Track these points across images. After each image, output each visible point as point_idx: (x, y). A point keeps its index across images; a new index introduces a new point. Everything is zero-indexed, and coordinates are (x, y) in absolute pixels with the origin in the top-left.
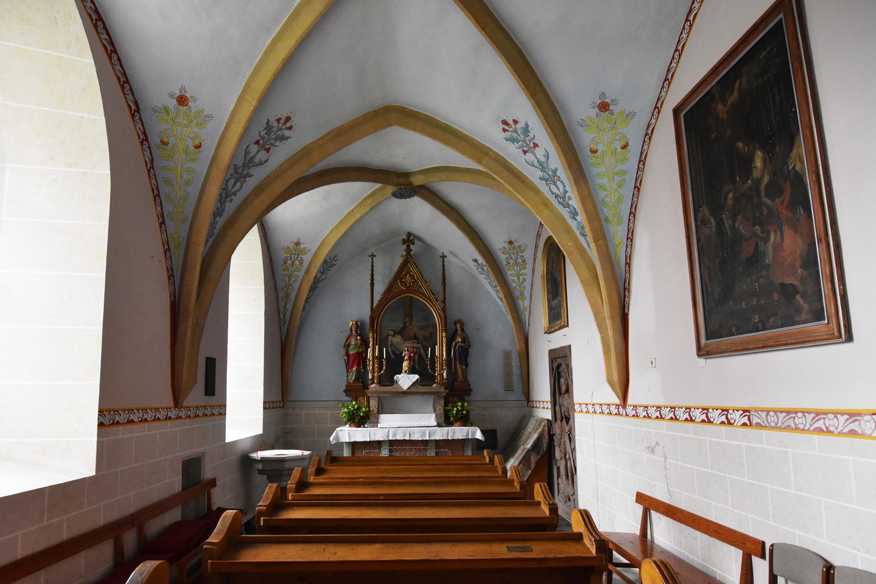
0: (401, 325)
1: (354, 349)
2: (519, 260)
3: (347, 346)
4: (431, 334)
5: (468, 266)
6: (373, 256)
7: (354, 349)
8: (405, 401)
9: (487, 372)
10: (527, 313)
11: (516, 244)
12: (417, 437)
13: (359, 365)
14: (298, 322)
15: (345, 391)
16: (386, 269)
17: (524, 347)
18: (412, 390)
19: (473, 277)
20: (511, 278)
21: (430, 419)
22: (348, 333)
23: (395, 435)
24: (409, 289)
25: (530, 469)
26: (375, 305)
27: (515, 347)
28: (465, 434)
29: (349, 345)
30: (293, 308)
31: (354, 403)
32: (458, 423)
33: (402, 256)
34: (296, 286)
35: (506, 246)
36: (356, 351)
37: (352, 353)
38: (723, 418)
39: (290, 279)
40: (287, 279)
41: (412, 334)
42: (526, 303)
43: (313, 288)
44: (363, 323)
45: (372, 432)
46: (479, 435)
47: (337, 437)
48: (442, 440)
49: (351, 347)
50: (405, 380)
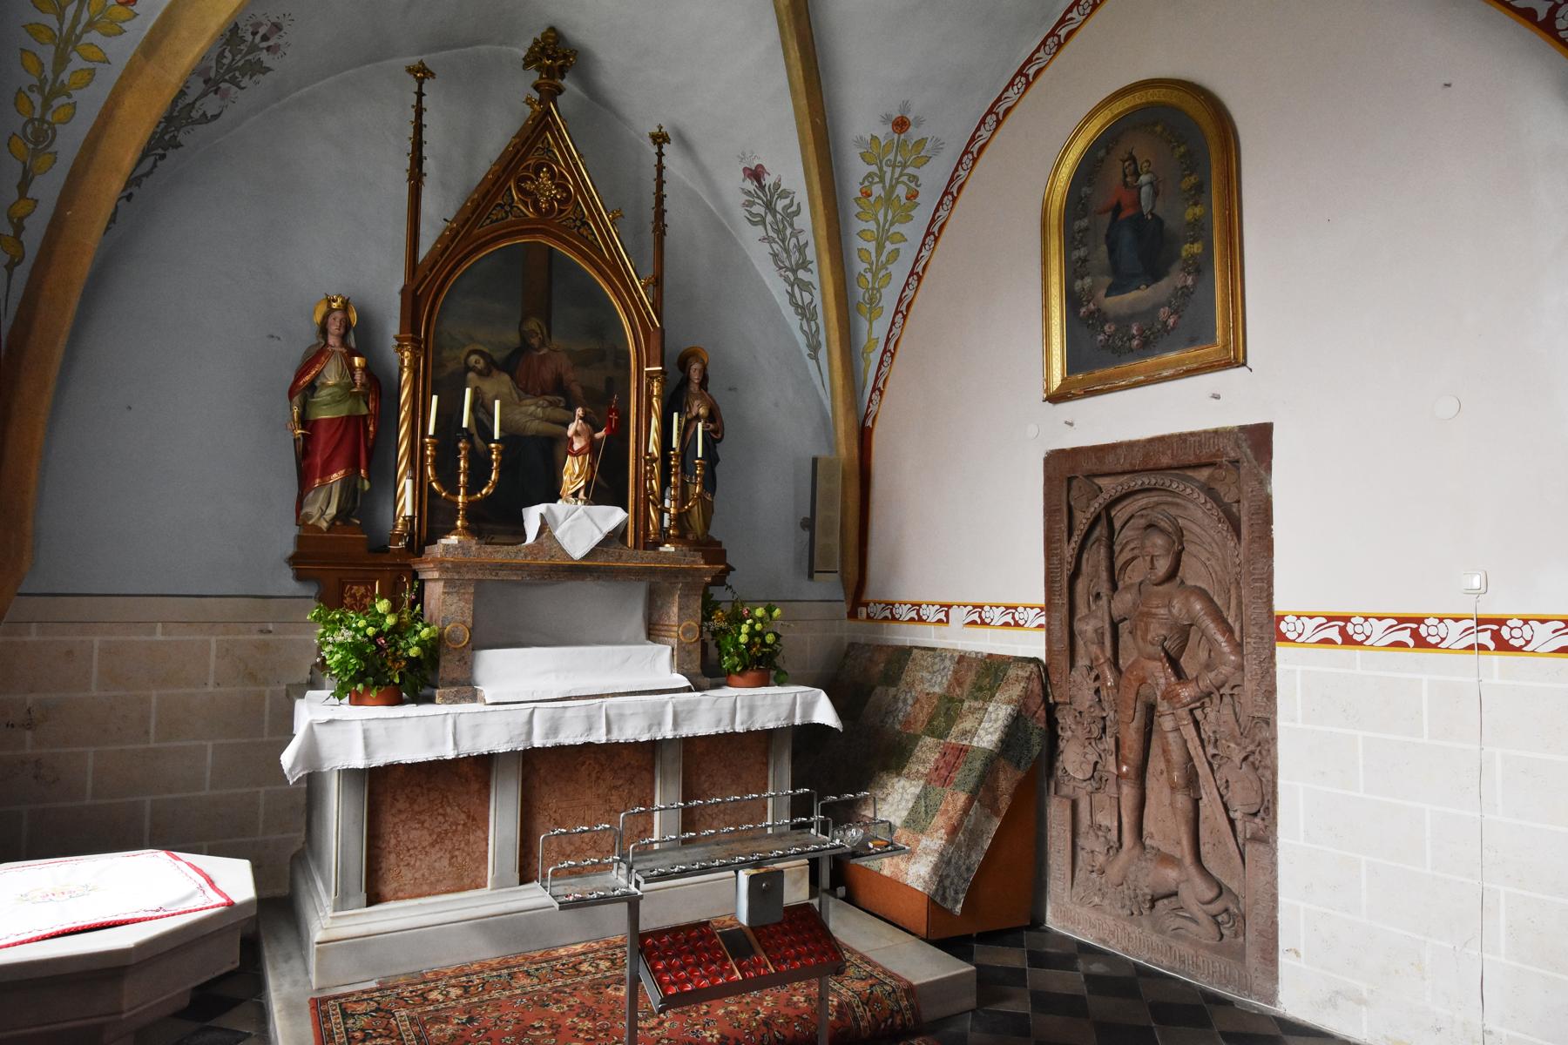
0: (513, 338)
1: (336, 401)
2: (901, 191)
3: (304, 390)
4: (610, 381)
5: (716, 194)
6: (422, 73)
7: (336, 401)
8: (549, 602)
9: (765, 508)
10: (875, 358)
11: (914, 133)
12: (633, 731)
13: (353, 465)
14: (83, 268)
15: (294, 561)
16: (475, 132)
17: (856, 451)
18: (600, 562)
19: (722, 232)
20: (859, 243)
21: (656, 665)
22: (310, 338)
23: (554, 729)
24: (547, 221)
25: (997, 814)
26: (423, 251)
27: (845, 449)
28: (784, 712)
29: (312, 387)
30: (57, 224)
31: (382, 606)
32: (751, 675)
33: (529, 102)
34: (90, 101)
35: (884, 132)
36: (342, 411)
37: (324, 414)
38: (913, 614)
39: (61, 61)
40: (47, 53)
41: (547, 374)
42: (880, 328)
43: (162, 143)
44: (356, 331)
45: (464, 724)
46: (824, 713)
47: (311, 752)
48: (717, 737)
49: (323, 395)
50: (577, 525)
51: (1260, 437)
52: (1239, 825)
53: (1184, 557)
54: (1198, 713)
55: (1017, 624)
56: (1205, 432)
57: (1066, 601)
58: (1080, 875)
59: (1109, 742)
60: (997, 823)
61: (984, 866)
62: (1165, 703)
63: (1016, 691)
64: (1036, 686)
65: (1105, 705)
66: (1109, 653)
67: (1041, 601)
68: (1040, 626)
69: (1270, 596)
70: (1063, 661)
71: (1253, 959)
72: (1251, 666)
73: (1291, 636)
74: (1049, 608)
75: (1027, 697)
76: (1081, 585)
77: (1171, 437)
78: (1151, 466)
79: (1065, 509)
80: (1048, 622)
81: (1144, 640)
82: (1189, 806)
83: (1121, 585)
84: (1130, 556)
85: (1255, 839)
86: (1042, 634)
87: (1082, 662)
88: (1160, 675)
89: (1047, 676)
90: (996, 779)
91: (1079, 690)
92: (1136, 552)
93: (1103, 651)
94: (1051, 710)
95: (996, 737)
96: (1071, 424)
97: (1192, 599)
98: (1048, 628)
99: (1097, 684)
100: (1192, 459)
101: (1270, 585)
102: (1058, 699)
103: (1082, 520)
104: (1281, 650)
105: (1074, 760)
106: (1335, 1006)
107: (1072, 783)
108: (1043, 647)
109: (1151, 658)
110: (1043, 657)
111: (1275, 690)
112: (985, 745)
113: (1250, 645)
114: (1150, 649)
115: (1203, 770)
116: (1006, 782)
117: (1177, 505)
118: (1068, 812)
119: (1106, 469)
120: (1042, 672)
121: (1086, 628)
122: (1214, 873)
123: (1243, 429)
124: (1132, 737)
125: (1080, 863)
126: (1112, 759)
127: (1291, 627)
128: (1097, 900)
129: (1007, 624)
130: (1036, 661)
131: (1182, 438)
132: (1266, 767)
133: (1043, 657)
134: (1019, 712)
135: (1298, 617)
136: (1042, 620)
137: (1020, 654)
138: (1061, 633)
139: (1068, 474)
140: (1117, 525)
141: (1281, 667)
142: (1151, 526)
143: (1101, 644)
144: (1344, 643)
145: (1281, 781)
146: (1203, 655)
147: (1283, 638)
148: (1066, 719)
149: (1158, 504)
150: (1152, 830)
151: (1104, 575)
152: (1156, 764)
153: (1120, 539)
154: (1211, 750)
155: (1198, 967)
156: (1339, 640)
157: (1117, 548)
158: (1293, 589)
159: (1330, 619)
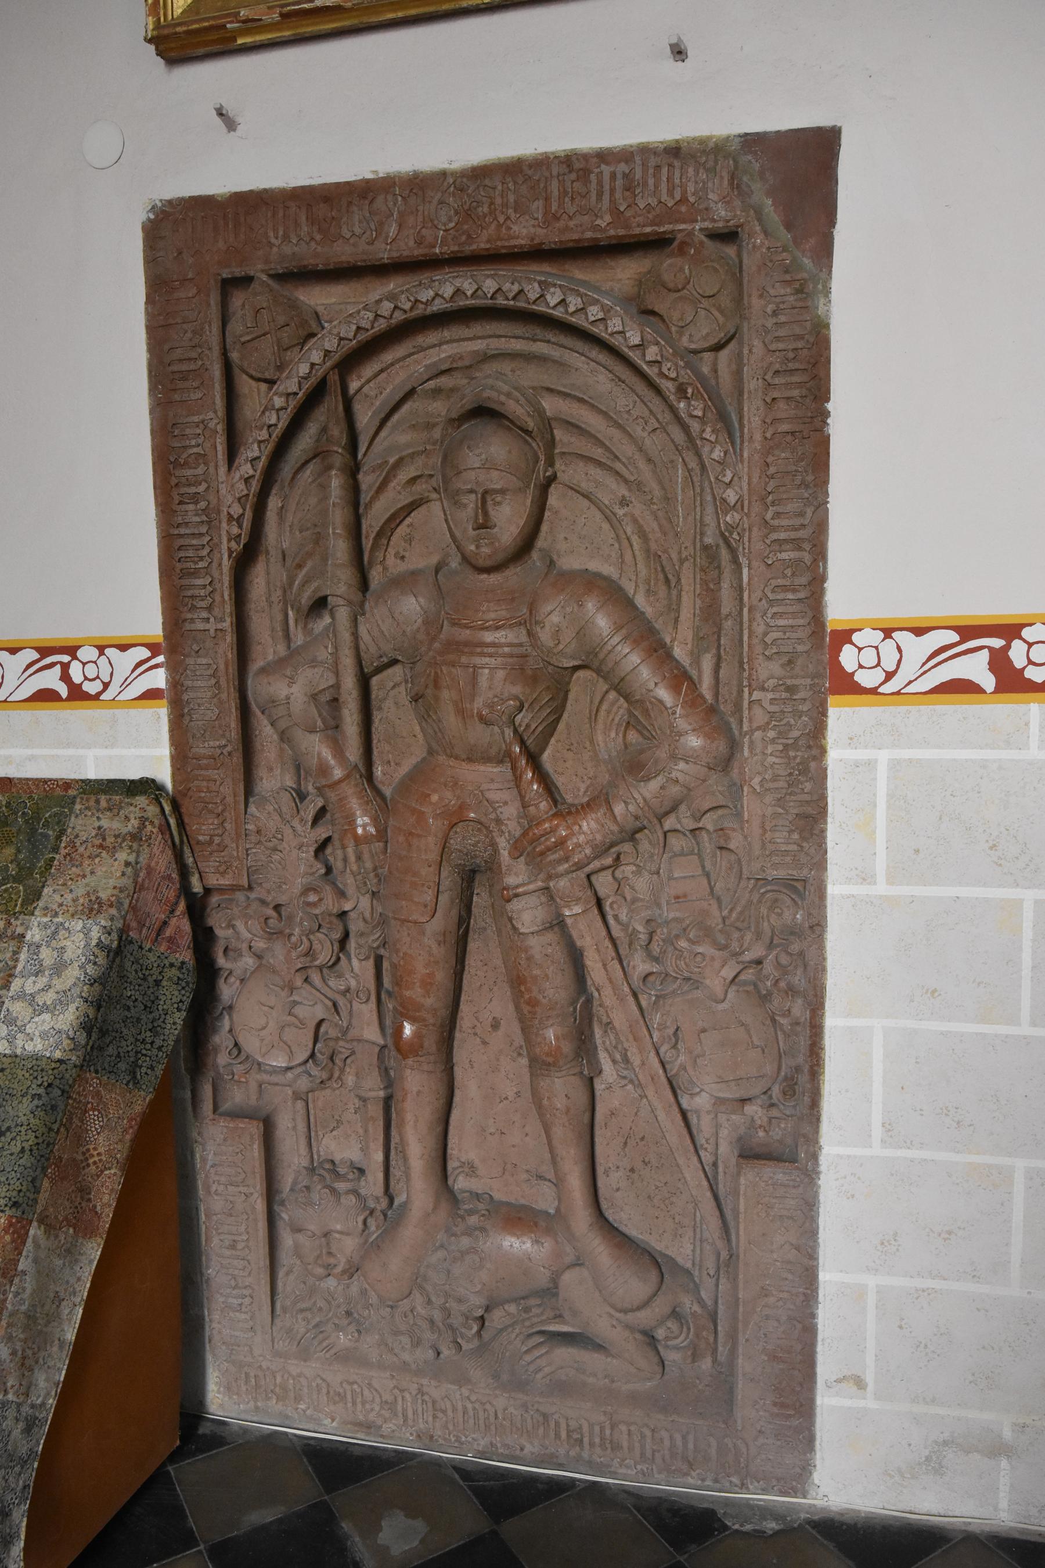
25: (83, 1227)
51: (805, 165)
52: (704, 1126)
53: (553, 500)
54: (604, 883)
55: (77, 694)
56: (645, 150)
57: (227, 624)
58: (287, 1284)
59: (358, 970)
60: (93, 1251)
61: (70, 1393)
62: (521, 865)
63: (108, 876)
64: (163, 861)
65: (349, 882)
66: (353, 752)
67: (153, 626)
68: (151, 695)
69: (817, 582)
70: (227, 785)
71: (752, 1405)
72: (761, 758)
73: (866, 679)
74: (175, 643)
75: (138, 887)
76: (261, 581)
77: (542, 163)
78: (481, 244)
79: (217, 371)
80: (175, 683)
81: (461, 712)
82: (580, 1097)
83: (376, 576)
84: (405, 500)
85: (751, 1154)
86: (160, 714)
87: (273, 779)
88: (494, 790)
89: (181, 824)
90: (79, 1139)
91: (273, 850)
92: (421, 488)
93: (339, 751)
94: (197, 909)
95: (68, 1018)
96: (230, 124)
97: (590, 606)
98: (177, 699)
99: (322, 832)
100: (604, 226)
101: (819, 552)
102: (213, 881)
103: (265, 409)
104: (842, 717)
105: (262, 1023)
106: (939, 1470)
107: (255, 1077)
108: (164, 751)
109: (475, 756)
110: (164, 775)
111: (823, 811)
112: (36, 1046)
113: (759, 708)
114: (479, 735)
115: (614, 1007)
116: (107, 1142)
117: (542, 359)
118: (256, 1151)
119: (344, 253)
120: (169, 812)
121: (288, 694)
122: (633, 1232)
123: (752, 142)
124: (423, 950)
125: (286, 1258)
126: (367, 1011)
127: (869, 657)
128: (343, 1340)
129: (46, 696)
130: (146, 786)
131: (577, 167)
132: (791, 991)
133: (164, 775)
134: (123, 932)
135: (888, 633)
136: (159, 679)
137: (92, 774)
138: (213, 706)
139: (214, 266)
140: (365, 417)
141: (837, 755)
142: (483, 413)
143: (333, 728)
144: (1002, 688)
145: (832, 1021)
146: (608, 741)
147: (846, 685)
148: (236, 928)
149: (486, 358)
150: (472, 1155)
151: (340, 548)
152: (486, 1002)
153: (376, 453)
154: (640, 966)
155: (616, 1447)
156: (988, 681)
157: (367, 480)
158: (876, 565)
159: (967, 632)
